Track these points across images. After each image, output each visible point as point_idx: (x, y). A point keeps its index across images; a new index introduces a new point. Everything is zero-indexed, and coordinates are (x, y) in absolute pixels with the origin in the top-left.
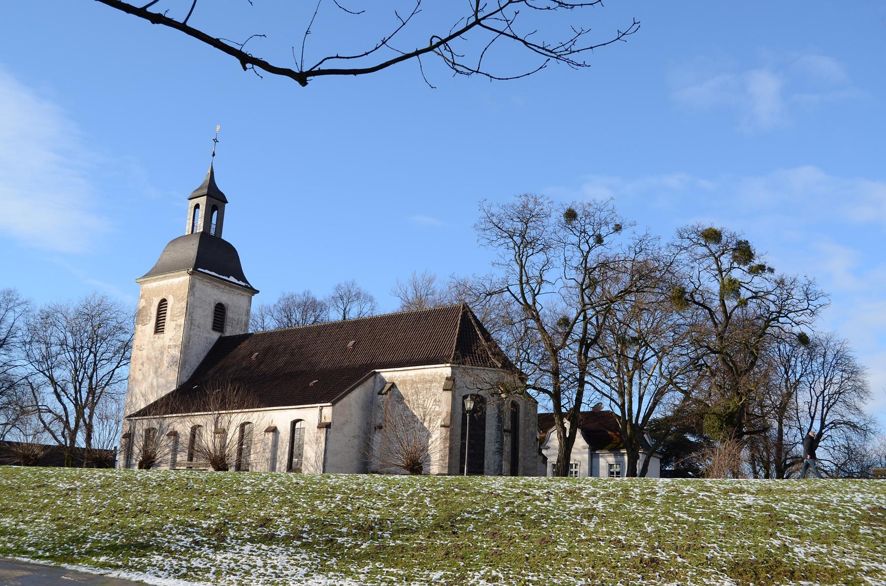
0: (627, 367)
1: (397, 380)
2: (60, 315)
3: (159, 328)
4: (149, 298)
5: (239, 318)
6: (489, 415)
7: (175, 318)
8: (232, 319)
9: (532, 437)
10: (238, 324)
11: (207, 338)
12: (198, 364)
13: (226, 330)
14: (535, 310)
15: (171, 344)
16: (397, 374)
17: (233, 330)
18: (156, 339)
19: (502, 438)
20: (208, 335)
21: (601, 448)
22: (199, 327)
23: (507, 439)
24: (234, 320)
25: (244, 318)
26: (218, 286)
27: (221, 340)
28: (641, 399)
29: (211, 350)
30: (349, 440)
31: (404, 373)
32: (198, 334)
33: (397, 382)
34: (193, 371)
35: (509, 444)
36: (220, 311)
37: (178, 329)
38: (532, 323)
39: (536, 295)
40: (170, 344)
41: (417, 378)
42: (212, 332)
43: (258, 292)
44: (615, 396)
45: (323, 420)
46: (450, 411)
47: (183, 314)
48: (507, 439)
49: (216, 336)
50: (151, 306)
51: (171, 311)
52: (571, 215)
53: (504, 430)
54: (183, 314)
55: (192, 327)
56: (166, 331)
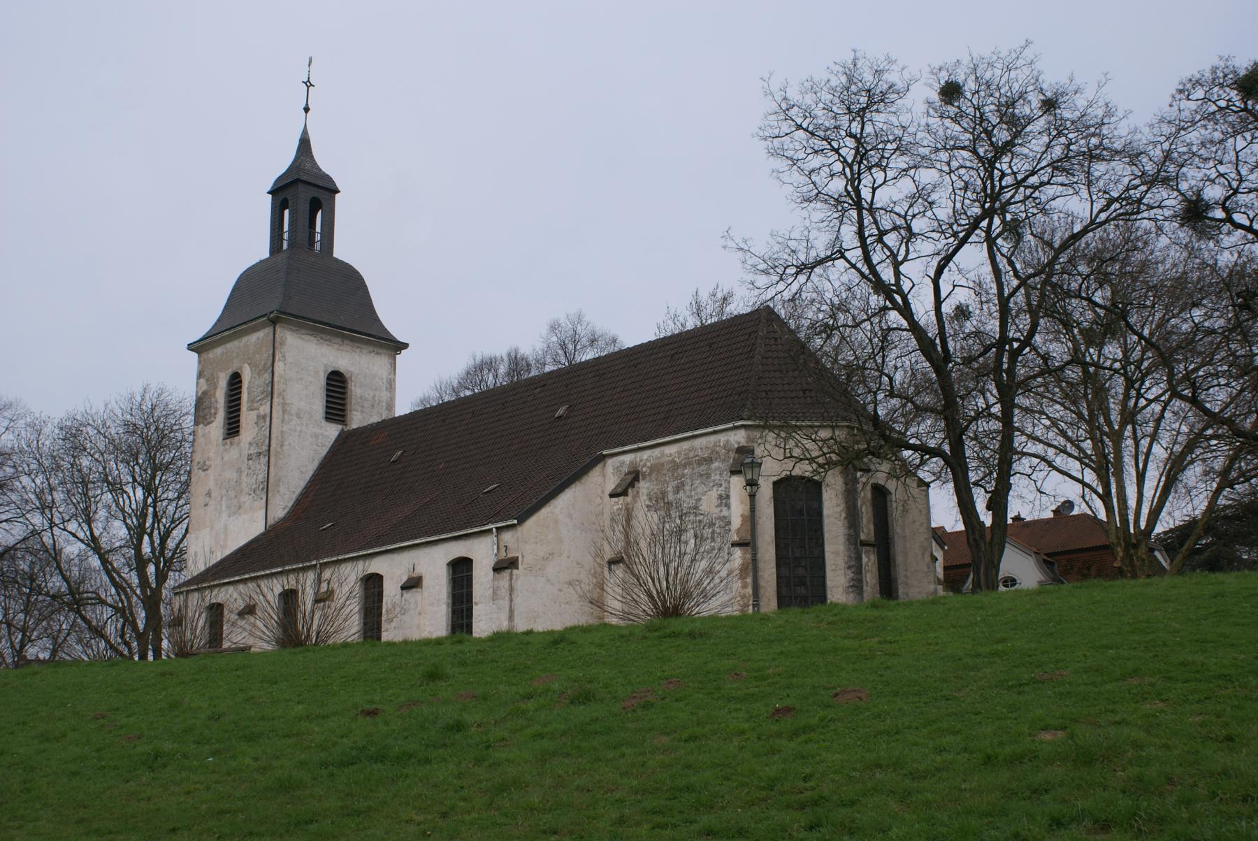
0: (1109, 423)
2: (92, 432)
3: (233, 428)
4: (212, 375)
5: (374, 396)
8: (361, 398)
9: (923, 555)
10: (373, 406)
11: (316, 436)
12: (303, 484)
13: (351, 419)
16: (645, 455)
17: (364, 418)
18: (228, 446)
19: (859, 559)
20: (318, 431)
22: (298, 416)
23: (869, 559)
25: (384, 395)
27: (344, 440)
28: (1141, 478)
29: (325, 457)
30: (561, 590)
31: (656, 452)
32: (298, 428)
34: (294, 497)
35: (875, 570)
36: (337, 384)
38: (894, 317)
39: (902, 263)
40: (251, 452)
43: (405, 346)
44: (1090, 477)
45: (503, 555)
47: (267, 396)
48: (869, 559)
50: (215, 389)
51: (249, 393)
52: (951, 92)
53: (861, 541)
54: (267, 396)
55: (286, 417)
56: (242, 430)
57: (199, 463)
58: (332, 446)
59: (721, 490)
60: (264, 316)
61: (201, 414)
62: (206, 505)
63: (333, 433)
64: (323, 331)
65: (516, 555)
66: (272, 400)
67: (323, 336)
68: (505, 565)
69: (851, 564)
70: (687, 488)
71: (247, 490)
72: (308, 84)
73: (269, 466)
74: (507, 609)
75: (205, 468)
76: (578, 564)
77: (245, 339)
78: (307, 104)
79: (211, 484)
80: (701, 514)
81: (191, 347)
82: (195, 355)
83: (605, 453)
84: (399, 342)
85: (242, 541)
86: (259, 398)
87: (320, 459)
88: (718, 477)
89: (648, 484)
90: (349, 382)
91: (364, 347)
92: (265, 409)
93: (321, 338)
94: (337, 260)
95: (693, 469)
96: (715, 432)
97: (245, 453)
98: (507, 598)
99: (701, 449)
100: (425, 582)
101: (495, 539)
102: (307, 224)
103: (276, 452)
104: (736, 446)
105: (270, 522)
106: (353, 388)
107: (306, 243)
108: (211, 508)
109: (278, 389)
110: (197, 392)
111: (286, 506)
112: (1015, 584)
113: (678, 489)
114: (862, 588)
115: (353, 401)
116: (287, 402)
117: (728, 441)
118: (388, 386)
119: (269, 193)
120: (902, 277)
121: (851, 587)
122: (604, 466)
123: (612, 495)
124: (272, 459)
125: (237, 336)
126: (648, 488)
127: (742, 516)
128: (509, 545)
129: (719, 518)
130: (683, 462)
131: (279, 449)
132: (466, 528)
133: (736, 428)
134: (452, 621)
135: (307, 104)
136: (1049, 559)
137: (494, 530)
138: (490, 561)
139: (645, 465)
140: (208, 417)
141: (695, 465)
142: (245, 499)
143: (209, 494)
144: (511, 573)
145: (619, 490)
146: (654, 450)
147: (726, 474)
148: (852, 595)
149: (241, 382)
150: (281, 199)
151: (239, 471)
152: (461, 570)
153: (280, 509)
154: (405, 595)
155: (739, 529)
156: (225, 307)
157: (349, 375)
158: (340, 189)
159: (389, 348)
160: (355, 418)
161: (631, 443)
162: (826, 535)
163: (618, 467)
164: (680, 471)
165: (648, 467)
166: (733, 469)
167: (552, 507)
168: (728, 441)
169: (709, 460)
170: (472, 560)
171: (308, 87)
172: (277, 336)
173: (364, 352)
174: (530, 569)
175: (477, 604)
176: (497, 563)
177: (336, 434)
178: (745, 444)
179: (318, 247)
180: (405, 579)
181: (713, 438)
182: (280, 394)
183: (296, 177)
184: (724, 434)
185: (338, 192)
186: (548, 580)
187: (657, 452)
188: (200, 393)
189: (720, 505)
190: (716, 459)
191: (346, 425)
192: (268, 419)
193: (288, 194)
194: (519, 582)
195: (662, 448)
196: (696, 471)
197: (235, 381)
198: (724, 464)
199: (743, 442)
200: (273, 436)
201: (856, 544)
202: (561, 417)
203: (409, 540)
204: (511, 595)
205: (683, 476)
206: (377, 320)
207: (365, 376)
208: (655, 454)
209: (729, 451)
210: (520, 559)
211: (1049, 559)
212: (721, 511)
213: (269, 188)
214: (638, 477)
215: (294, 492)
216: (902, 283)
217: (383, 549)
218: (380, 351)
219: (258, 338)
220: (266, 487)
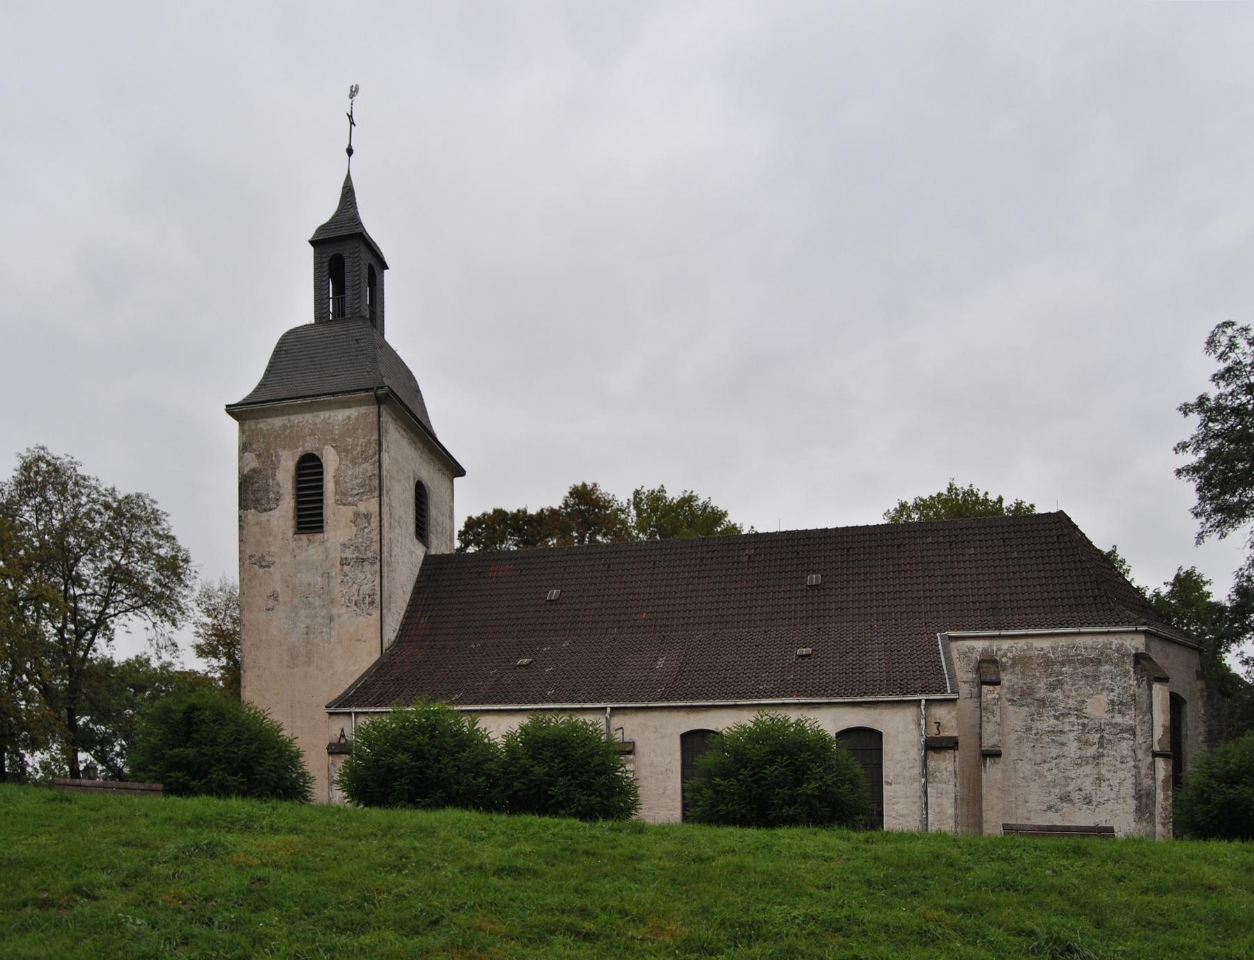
15: (349, 556)
16: (1006, 644)
41: (1059, 653)
51: (337, 483)
54: (371, 491)
66: (380, 496)
70: (1066, 687)
75: (264, 564)
78: (350, 145)
80: (1085, 717)
81: (232, 410)
82: (235, 424)
89: (1009, 677)
95: (1075, 668)
96: (1108, 633)
97: (336, 555)
104: (1133, 652)
113: (1052, 687)
117: (1122, 645)
126: (1010, 681)
127: (1163, 726)
128: (943, 722)
130: (1060, 659)
133: (1136, 632)
135: (350, 145)
137: (923, 702)
139: (1004, 655)
140: (264, 502)
146: (1017, 641)
150: (331, 255)
151: (327, 576)
168: (1122, 645)
169: (1097, 662)
170: (881, 733)
181: (1101, 640)
184: (1117, 636)
187: (1022, 643)
192: (375, 522)
195: (1030, 640)
197: (309, 469)
199: (1142, 649)
205: (1061, 674)
209: (1124, 656)
213: (310, 235)
217: (731, 702)
218: (446, 472)
219: (349, 418)
220: (379, 601)
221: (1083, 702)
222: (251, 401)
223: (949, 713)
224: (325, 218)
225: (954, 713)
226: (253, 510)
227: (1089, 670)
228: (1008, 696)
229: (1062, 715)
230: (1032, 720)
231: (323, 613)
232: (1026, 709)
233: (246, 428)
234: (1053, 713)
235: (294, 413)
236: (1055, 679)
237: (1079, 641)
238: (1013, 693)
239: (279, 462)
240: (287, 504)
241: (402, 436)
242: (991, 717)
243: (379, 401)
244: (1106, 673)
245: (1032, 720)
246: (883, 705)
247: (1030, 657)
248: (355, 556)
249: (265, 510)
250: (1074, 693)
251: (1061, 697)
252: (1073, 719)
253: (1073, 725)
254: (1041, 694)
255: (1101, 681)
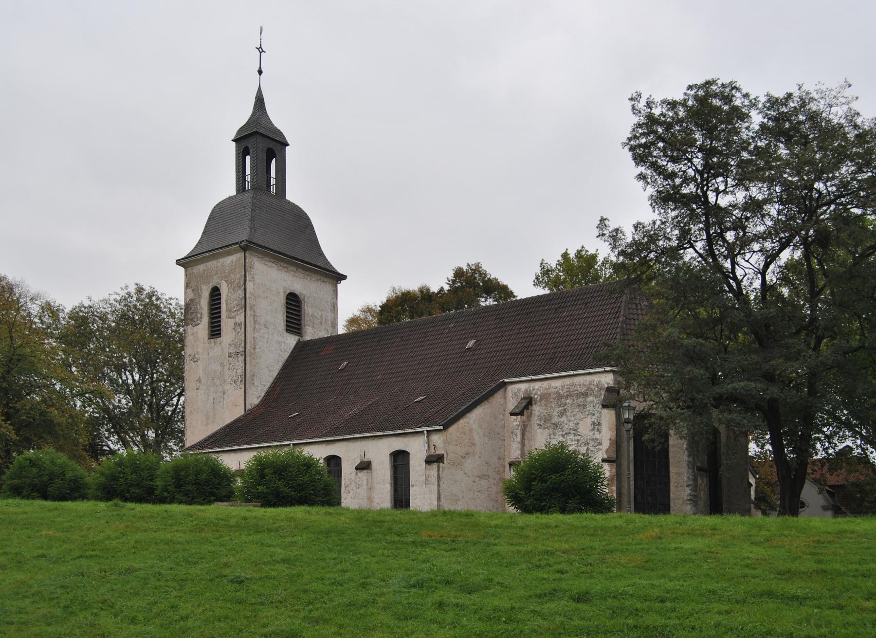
1: (536, 394)
3: (215, 331)
4: (197, 286)
5: (321, 317)
6: (674, 446)
7: (233, 314)
8: (312, 316)
10: (321, 323)
12: (271, 380)
14: (735, 278)
15: (232, 351)
16: (537, 385)
18: (212, 345)
21: (721, 207)
23: (703, 481)
24: (316, 317)
26: (287, 268)
27: (301, 347)
29: (287, 361)
30: (474, 482)
33: (536, 396)
34: (265, 389)
37: (238, 328)
41: (565, 390)
42: (286, 334)
43: (344, 277)
45: (432, 451)
46: (614, 438)
47: (241, 308)
49: (292, 341)
51: (227, 304)
54: (241, 308)
55: (257, 327)
56: (223, 334)
57: (190, 355)
58: (292, 352)
59: (594, 418)
60: (236, 244)
61: (190, 317)
62: (197, 389)
63: (293, 342)
64: (282, 260)
65: (443, 452)
67: (282, 264)
68: (434, 460)
69: (689, 483)
70: (568, 414)
71: (229, 380)
72: (261, 50)
73: (245, 364)
74: (436, 492)
75: (195, 360)
76: (487, 463)
77: (221, 261)
78: (260, 68)
79: (201, 373)
80: (579, 435)
81: (179, 262)
82: (182, 269)
83: (506, 380)
84: (339, 274)
85: (228, 421)
86: (235, 309)
87: (284, 362)
88: (592, 408)
89: (538, 408)
90: (303, 302)
91: (313, 275)
92: (240, 318)
93: (280, 265)
94: (289, 202)
95: (573, 400)
96: (590, 374)
97: (227, 351)
98: (436, 484)
99: (580, 385)
100: (374, 465)
101: (426, 439)
102: (265, 170)
103: (251, 353)
104: (606, 386)
105: (249, 407)
106: (306, 308)
107: (265, 186)
108: (201, 392)
109: (250, 304)
110: (185, 299)
111: (260, 396)
112: (804, 506)
113: (561, 414)
114: (697, 501)
115: (306, 318)
116: (257, 314)
117: (600, 382)
118: (332, 308)
119: (233, 141)
120: (736, 266)
121: (689, 500)
122: (505, 391)
123: (512, 414)
124: (248, 358)
125: (215, 257)
126: (539, 411)
127: (610, 439)
128: (437, 445)
129: (592, 439)
130: (566, 394)
131: (252, 351)
132: (404, 428)
133: (606, 372)
134: (394, 497)
135: (260, 68)
136: (831, 490)
138: (424, 456)
141: (575, 398)
142: (227, 387)
143: (199, 380)
144: (439, 465)
145: (517, 411)
146: (543, 383)
147: (599, 407)
148: (689, 506)
149: (220, 294)
151: (222, 365)
152: (400, 459)
153: (255, 397)
154: (359, 474)
155: (607, 450)
156: (204, 232)
157: (303, 297)
158: (289, 142)
159: (332, 278)
160: (308, 332)
161: (525, 375)
162: (671, 460)
163: (516, 393)
164: (563, 401)
165: (539, 395)
166: (604, 404)
167: (468, 418)
168: (600, 382)
169: (585, 395)
170: (408, 453)
171: (261, 53)
172: (247, 261)
173: (313, 279)
174: (453, 464)
175: (413, 486)
176: (428, 457)
177: (295, 343)
178: (612, 385)
179: (273, 189)
180: (358, 462)
182: (251, 308)
183: (255, 130)
184: (597, 376)
185: (288, 145)
186: (465, 474)
187: (545, 384)
188: (188, 300)
189: (593, 430)
190: (591, 394)
191: (302, 336)
192: (243, 326)
193: (250, 143)
194: (444, 473)
195: (550, 382)
196: (575, 401)
197: (215, 293)
198: (597, 399)
199: (611, 384)
200: (248, 341)
201: (693, 469)
202: (470, 348)
203: (360, 433)
204: (438, 482)
205: (566, 404)
206: (321, 254)
207: (315, 299)
208: (544, 385)
209: (601, 389)
210: (445, 456)
211: (831, 490)
212: (594, 434)
213: (233, 137)
214: (532, 402)
215: (265, 385)
216: (736, 271)
217: (341, 438)
218: (325, 280)
220: (244, 380)
221: (578, 424)
222: (193, 254)
223: (440, 438)
224: (243, 122)
225: (442, 438)
226: (190, 326)
227: (581, 400)
228: (538, 422)
229: (566, 434)
230: (550, 439)
231: (220, 389)
232: (547, 430)
233: (188, 273)
234: (561, 433)
235: (208, 261)
236: (562, 408)
237: (577, 380)
238: (540, 420)
239: (202, 293)
240: (205, 320)
241: (270, 267)
242: (515, 438)
243: (245, 249)
244: (590, 402)
245: (550, 439)
246: (410, 435)
247: (550, 394)
248: (234, 351)
249: (196, 325)
250: (573, 418)
251: (566, 421)
252: (572, 436)
253: (572, 441)
254: (555, 420)
255: (588, 408)
